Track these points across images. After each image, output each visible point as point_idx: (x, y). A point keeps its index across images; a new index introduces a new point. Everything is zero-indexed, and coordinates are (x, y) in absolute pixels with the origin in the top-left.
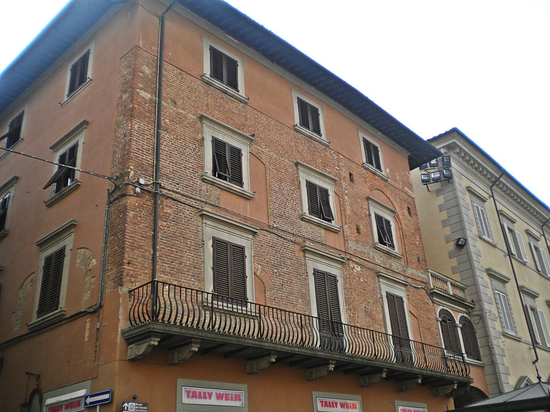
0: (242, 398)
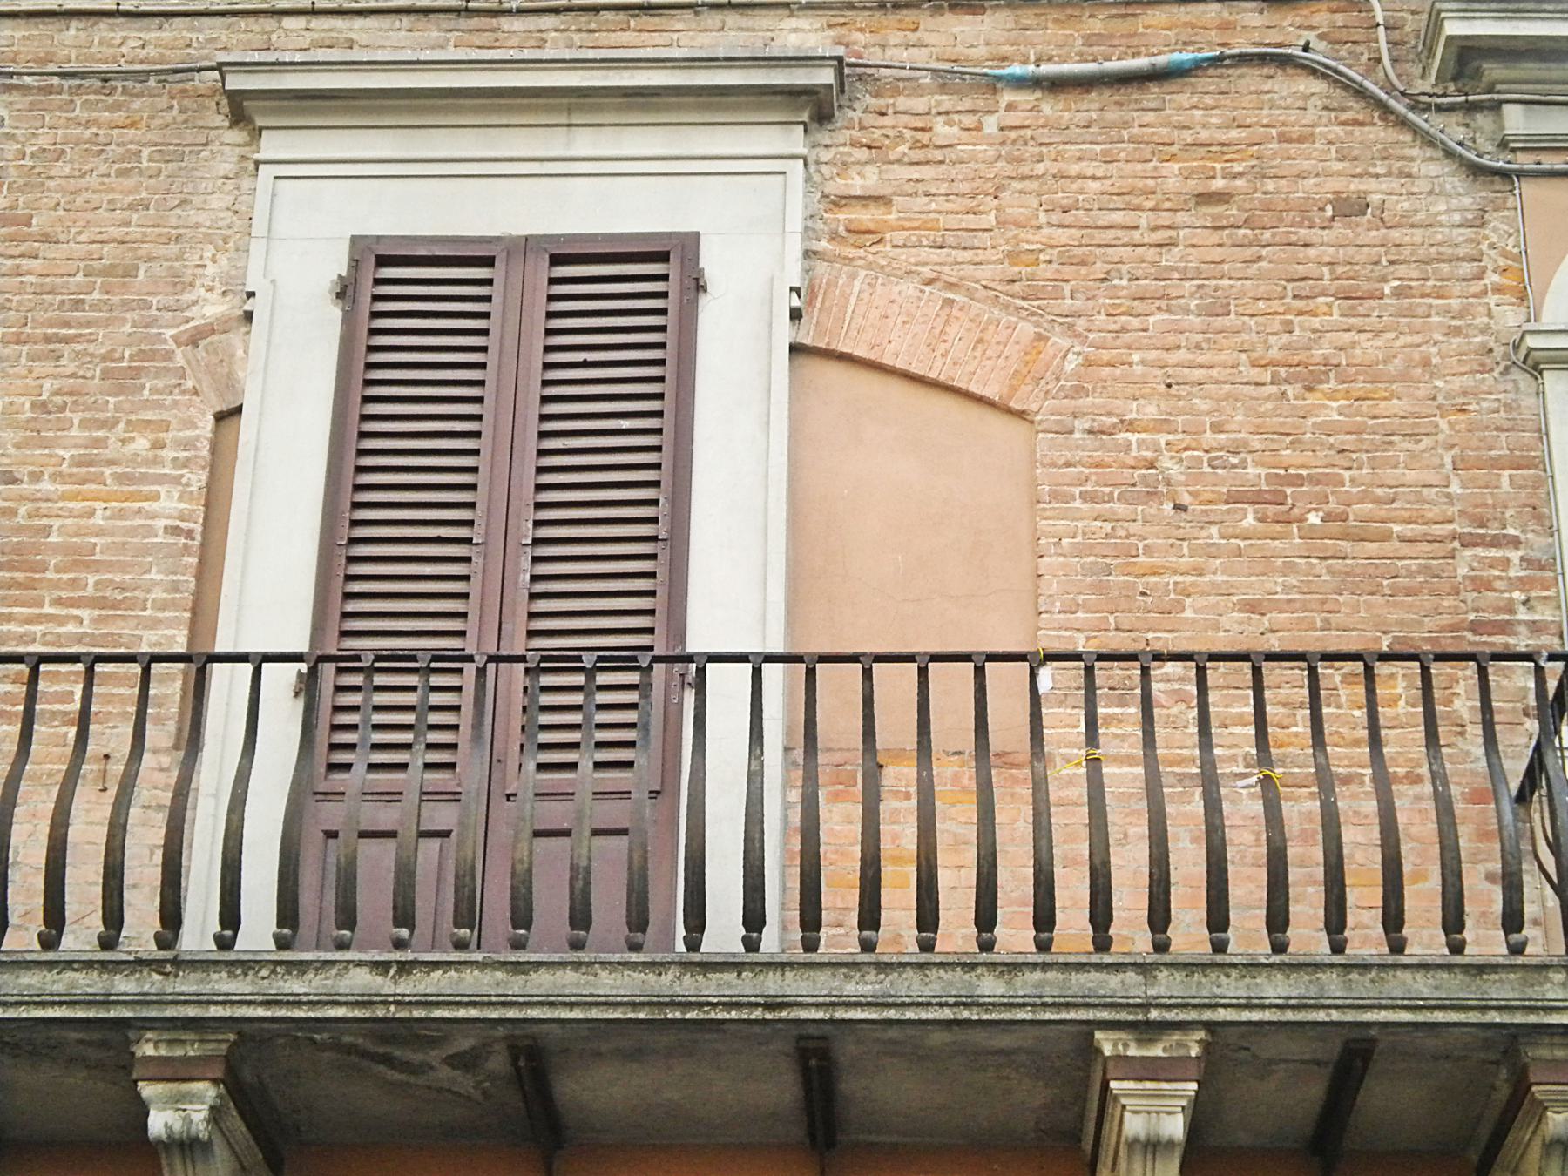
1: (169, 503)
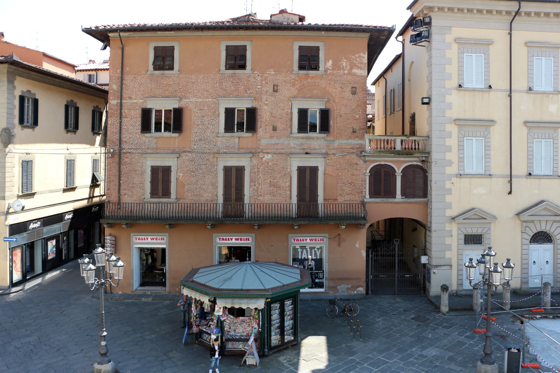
0: (165, 239)
1: (288, 184)
